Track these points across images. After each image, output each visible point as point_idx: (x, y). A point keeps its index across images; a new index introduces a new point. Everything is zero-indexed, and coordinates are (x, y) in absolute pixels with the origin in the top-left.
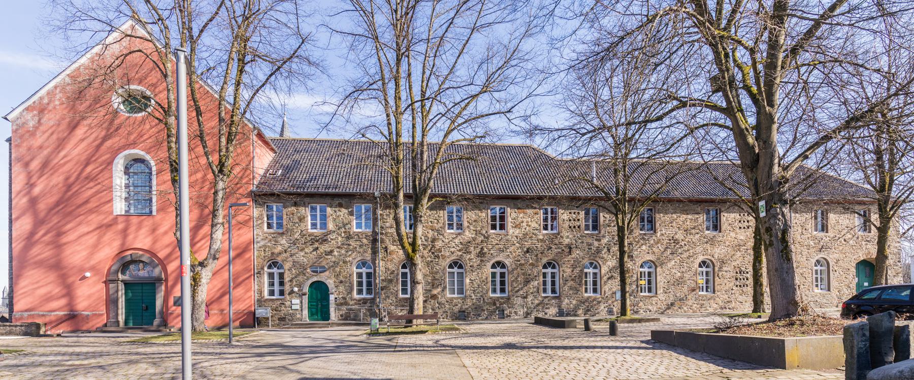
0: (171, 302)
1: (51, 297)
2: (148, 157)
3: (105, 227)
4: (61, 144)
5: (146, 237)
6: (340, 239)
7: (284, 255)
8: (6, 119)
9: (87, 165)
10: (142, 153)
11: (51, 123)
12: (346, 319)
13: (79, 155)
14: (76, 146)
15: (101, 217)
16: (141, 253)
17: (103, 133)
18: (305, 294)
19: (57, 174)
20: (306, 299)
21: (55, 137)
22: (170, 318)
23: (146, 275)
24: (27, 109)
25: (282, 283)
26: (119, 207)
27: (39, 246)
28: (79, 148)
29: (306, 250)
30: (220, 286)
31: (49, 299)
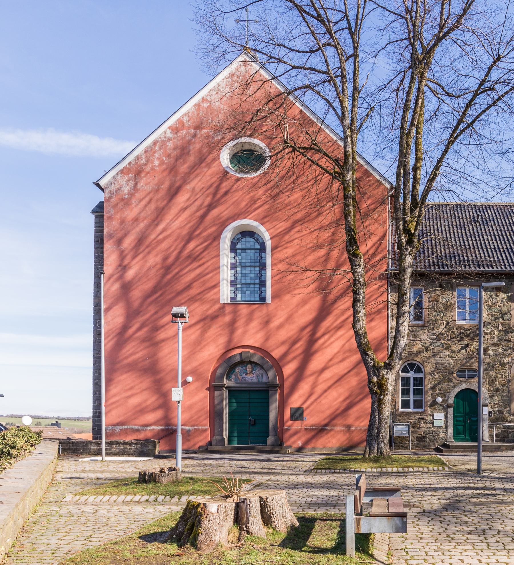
0: (287, 413)
1: (146, 407)
2: (262, 229)
3: (207, 320)
4: (160, 214)
5: (257, 333)
6: (496, 333)
7: (425, 354)
8: (98, 185)
9: (188, 241)
10: (255, 224)
11: (149, 188)
12: (502, 440)
13: (180, 228)
14: (178, 215)
15: (205, 307)
16: (251, 351)
17: (209, 200)
18: (449, 406)
19: (154, 253)
20: (451, 411)
21: (153, 206)
22: (286, 435)
23: (255, 380)
24: (122, 172)
25: (418, 392)
26: (226, 293)
27: (134, 344)
28: (181, 219)
29: (453, 348)
30: (346, 394)
31: (142, 411)
